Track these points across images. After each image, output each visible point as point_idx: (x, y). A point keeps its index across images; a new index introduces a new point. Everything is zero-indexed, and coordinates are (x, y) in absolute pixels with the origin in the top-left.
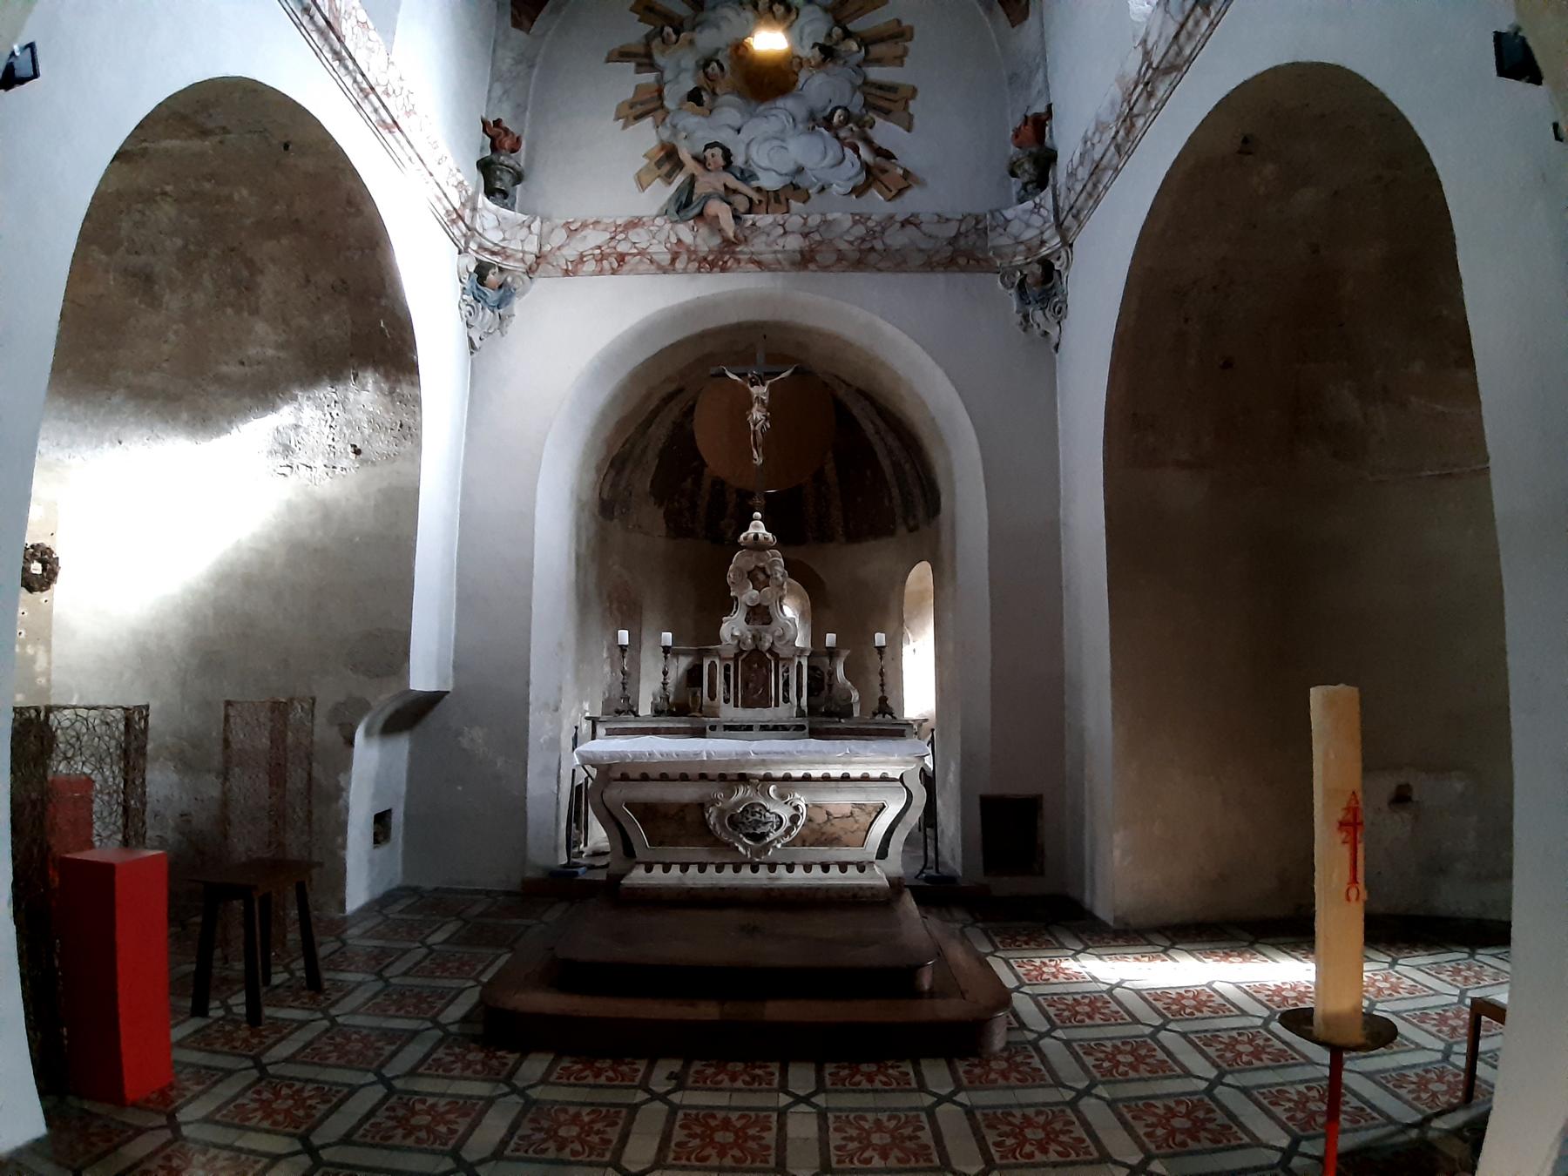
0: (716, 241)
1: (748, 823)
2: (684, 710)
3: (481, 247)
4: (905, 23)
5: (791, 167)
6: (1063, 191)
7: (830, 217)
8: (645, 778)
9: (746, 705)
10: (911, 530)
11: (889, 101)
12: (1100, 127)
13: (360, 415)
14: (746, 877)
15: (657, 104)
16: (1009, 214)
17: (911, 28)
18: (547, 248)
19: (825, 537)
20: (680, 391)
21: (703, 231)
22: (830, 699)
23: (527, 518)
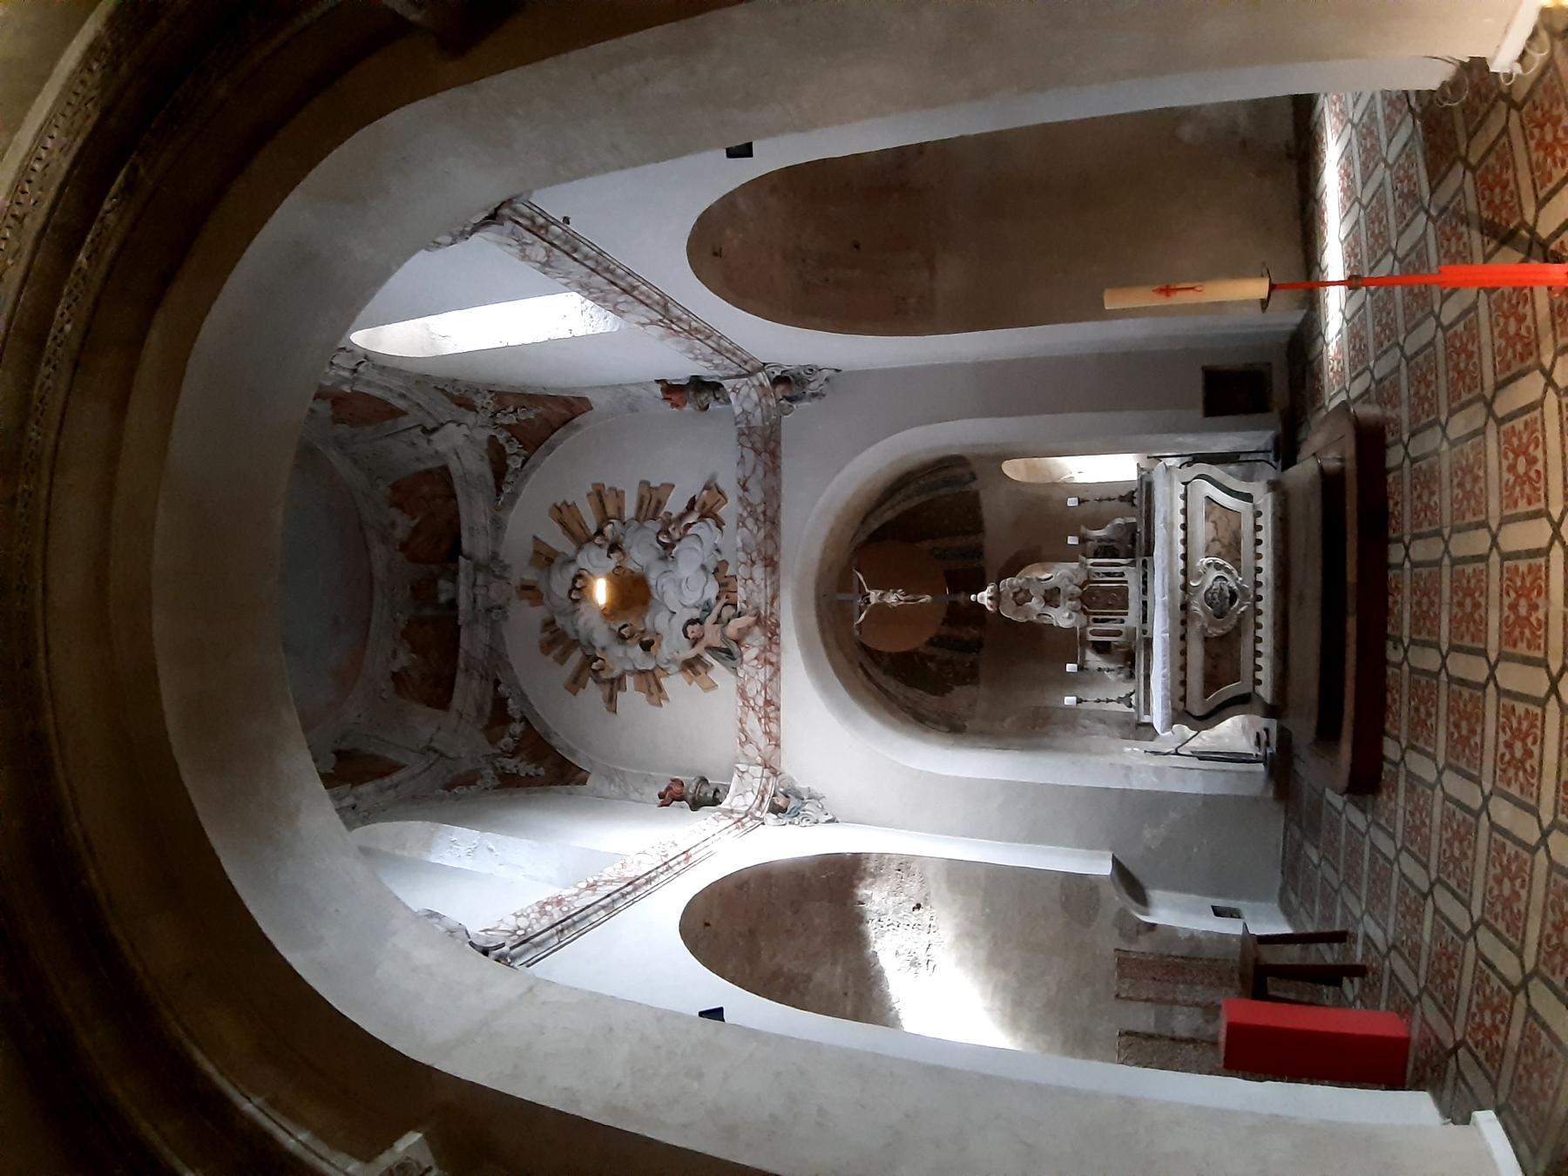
0: (757, 630)
1: (1222, 602)
2: (1129, 656)
3: (759, 808)
4: (590, 489)
5: (701, 574)
6: (726, 373)
7: (740, 544)
8: (1184, 683)
9: (1126, 607)
10: (974, 477)
11: (651, 502)
12: (690, 350)
13: (890, 902)
14: (1266, 605)
15: (650, 676)
16: (738, 411)
17: (594, 485)
18: (759, 760)
19: (978, 552)
20: (861, 666)
21: (748, 640)
22: (1120, 541)
23: (969, 785)
